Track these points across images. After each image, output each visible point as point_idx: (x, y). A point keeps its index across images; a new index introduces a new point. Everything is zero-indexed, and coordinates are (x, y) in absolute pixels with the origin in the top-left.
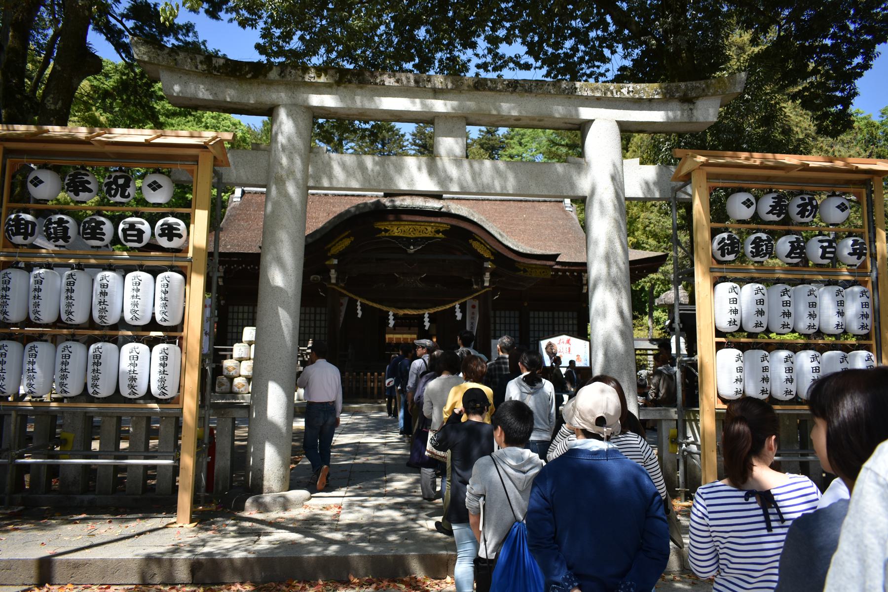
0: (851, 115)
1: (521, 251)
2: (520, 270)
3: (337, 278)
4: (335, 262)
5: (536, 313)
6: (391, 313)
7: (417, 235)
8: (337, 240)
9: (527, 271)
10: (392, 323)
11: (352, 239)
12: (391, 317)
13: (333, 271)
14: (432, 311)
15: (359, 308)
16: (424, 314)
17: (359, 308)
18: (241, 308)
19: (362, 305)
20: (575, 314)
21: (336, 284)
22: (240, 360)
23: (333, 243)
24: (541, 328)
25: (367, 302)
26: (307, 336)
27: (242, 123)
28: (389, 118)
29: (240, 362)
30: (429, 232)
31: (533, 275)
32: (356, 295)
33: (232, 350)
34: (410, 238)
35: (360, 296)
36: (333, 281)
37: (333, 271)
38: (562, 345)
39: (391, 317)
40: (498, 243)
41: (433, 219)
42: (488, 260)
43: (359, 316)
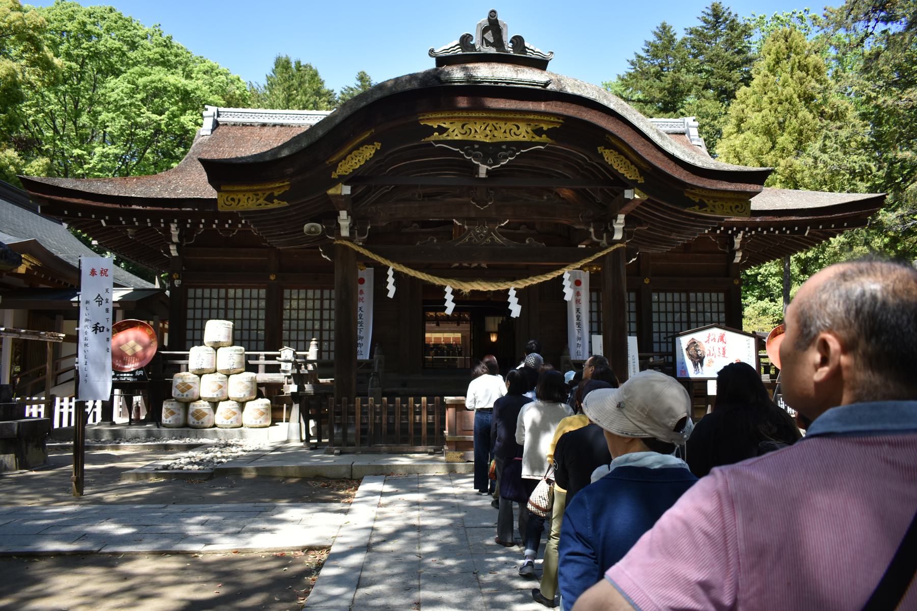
1: (699, 164)
2: (693, 204)
3: (351, 229)
4: (346, 190)
5: (662, 295)
6: (449, 290)
8: (349, 148)
10: (450, 306)
11: (378, 145)
12: (449, 297)
13: (343, 214)
14: (522, 284)
15: (391, 280)
16: (508, 290)
17: (391, 280)
18: (207, 292)
19: (397, 274)
20: (722, 296)
21: (350, 239)
22: (200, 374)
23: (342, 154)
25: (406, 270)
26: (309, 334)
27: (241, 79)
29: (228, 376)
30: (523, 133)
32: (386, 258)
33: (185, 357)
35: (393, 261)
36: (345, 233)
37: (343, 214)
38: (712, 344)
39: (449, 297)
40: (655, 151)
41: (530, 106)
42: (631, 185)
43: (391, 295)
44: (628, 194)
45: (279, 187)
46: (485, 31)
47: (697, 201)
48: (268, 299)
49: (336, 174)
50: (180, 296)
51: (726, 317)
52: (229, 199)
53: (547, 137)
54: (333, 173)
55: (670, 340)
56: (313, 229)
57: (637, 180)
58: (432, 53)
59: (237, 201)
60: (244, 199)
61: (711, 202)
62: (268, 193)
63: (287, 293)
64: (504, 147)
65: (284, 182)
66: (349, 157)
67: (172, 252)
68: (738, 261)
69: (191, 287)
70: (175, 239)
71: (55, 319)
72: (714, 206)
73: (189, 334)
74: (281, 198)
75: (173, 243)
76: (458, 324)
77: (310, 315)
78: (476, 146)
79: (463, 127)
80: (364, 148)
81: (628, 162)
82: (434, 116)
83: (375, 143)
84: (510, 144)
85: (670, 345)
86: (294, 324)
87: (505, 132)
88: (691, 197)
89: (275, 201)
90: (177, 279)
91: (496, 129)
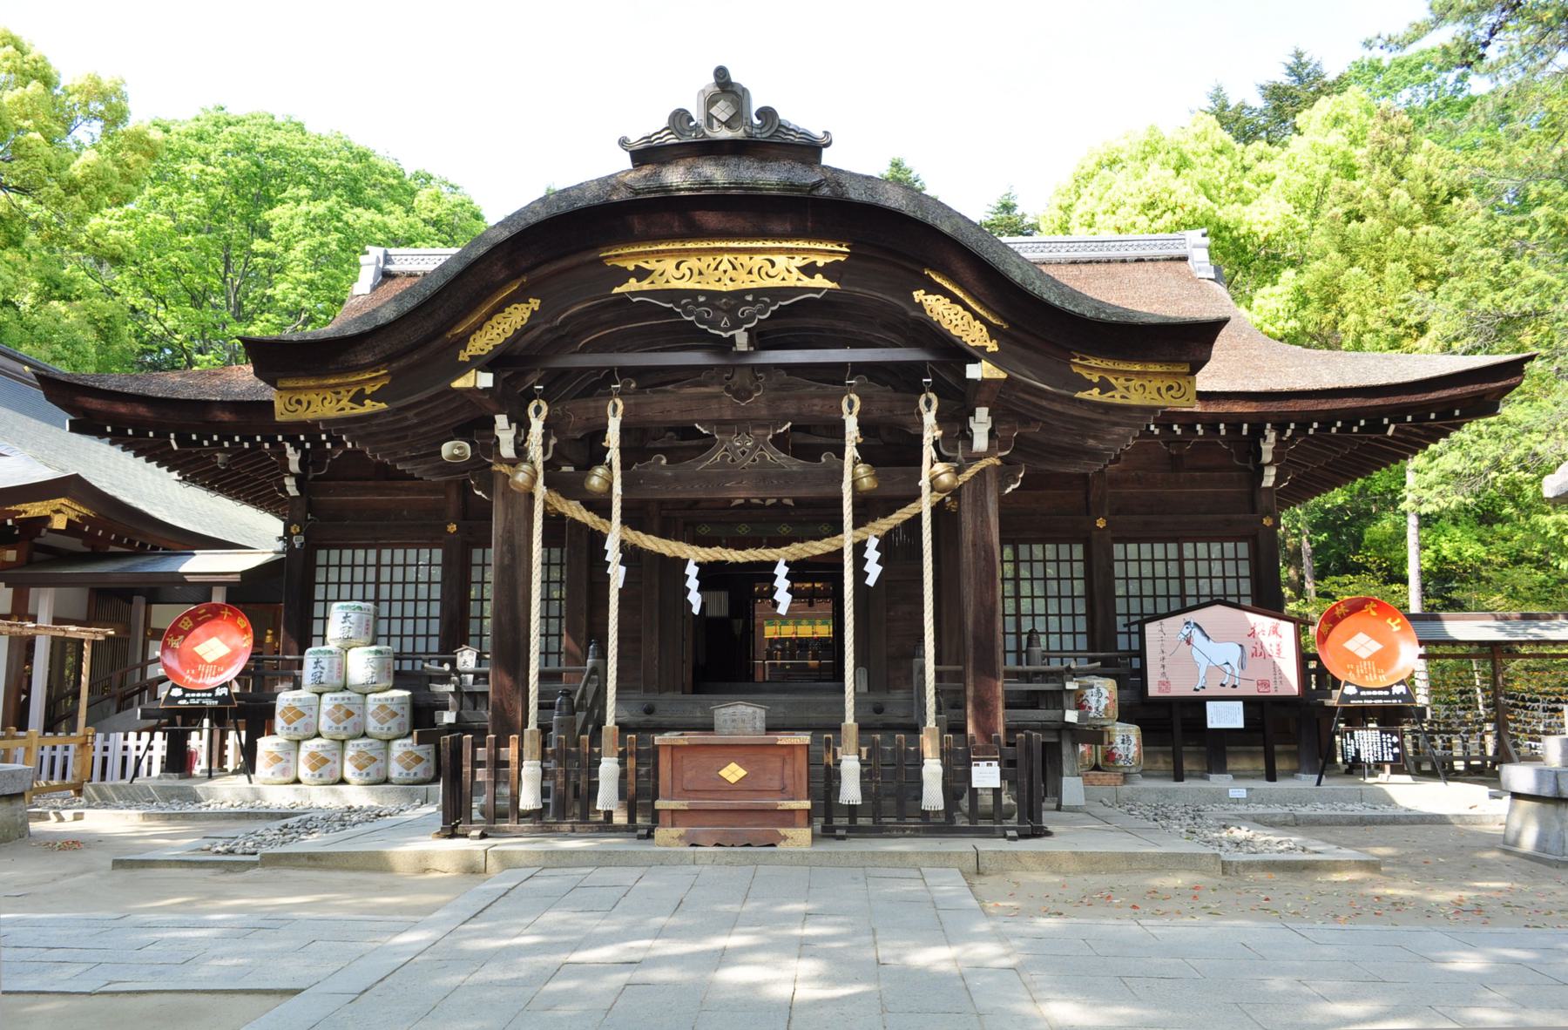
2: (1090, 385)
4: (486, 380)
9: (1112, 388)
11: (535, 304)
16: (774, 564)
20: (1243, 549)
23: (473, 319)
37: (982, 413)
44: (974, 371)
45: (373, 381)
46: (711, 102)
47: (1096, 380)
48: (446, 565)
49: (988, 344)
52: (293, 401)
53: (824, 277)
54: (462, 352)
55: (1135, 628)
56: (456, 452)
57: (986, 347)
58: (623, 142)
59: (305, 405)
61: (1122, 380)
62: (355, 390)
64: (749, 298)
65: (378, 371)
66: (487, 326)
67: (288, 489)
68: (1270, 484)
69: (322, 547)
70: (294, 467)
71: (131, 603)
72: (1127, 388)
74: (375, 397)
76: (811, 604)
77: (1160, 569)
78: (702, 299)
79: (678, 267)
80: (511, 309)
81: (968, 315)
82: (626, 251)
83: (531, 300)
84: (759, 293)
85: (1135, 638)
86: (1134, 588)
87: (750, 272)
88: (1084, 373)
89: (367, 402)
90: (298, 534)
91: (734, 268)
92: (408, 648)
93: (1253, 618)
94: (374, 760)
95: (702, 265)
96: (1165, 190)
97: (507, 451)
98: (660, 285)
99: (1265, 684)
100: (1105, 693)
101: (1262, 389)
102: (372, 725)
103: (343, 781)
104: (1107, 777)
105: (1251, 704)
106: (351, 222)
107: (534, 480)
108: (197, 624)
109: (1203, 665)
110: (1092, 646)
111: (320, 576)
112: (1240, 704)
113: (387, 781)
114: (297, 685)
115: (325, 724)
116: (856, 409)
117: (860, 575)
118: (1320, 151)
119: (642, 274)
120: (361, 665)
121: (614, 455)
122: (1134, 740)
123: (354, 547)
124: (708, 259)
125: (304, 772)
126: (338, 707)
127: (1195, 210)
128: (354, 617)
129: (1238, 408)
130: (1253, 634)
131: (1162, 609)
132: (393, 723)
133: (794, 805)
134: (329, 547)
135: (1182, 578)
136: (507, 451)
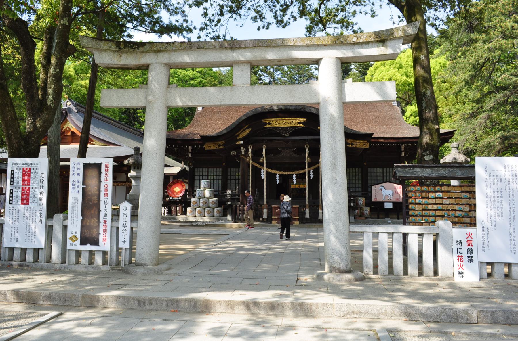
0: (179, 34)
4: (242, 142)
7: (288, 125)
8: (242, 130)
9: (354, 145)
11: (250, 129)
13: (242, 148)
14: (297, 172)
16: (293, 175)
24: (379, 178)
28: (307, 62)
31: (358, 147)
34: (283, 127)
37: (242, 148)
45: (222, 143)
48: (222, 172)
50: (192, 171)
51: (368, 182)
60: (212, 146)
63: (229, 170)
69: (196, 168)
70: (190, 151)
73: (195, 185)
74: (222, 146)
75: (190, 153)
84: (290, 127)
92: (217, 190)
93: (395, 185)
94: (211, 212)
95: (280, 122)
96: (393, 75)
97: (243, 153)
98: (273, 126)
99: (397, 199)
100: (362, 200)
101: (397, 137)
102: (211, 205)
103: (205, 216)
104: (362, 218)
105: (394, 203)
106: (179, 74)
107: (250, 160)
108: (174, 184)
109: (384, 195)
110: (362, 191)
111: (196, 174)
112: (392, 203)
113: (214, 216)
114: (194, 197)
115: (201, 205)
116: (308, 147)
117: (309, 177)
118: (438, 63)
119: (269, 124)
120: (207, 193)
121: (264, 155)
122: (368, 210)
123: (203, 168)
124: (281, 121)
125: (197, 214)
126: (204, 201)
127: (401, 81)
128: (206, 183)
129: (392, 141)
130: (395, 189)
131: (375, 183)
132: (215, 205)
133: (296, 217)
134: (197, 168)
135: (383, 176)
136: (243, 153)
